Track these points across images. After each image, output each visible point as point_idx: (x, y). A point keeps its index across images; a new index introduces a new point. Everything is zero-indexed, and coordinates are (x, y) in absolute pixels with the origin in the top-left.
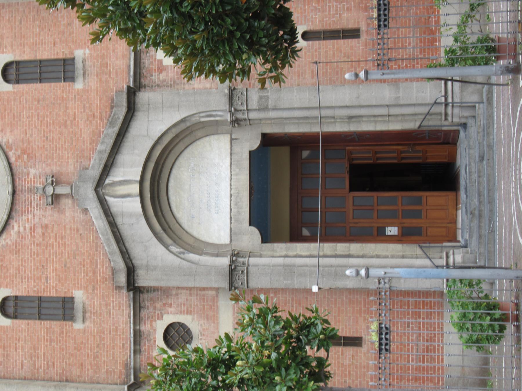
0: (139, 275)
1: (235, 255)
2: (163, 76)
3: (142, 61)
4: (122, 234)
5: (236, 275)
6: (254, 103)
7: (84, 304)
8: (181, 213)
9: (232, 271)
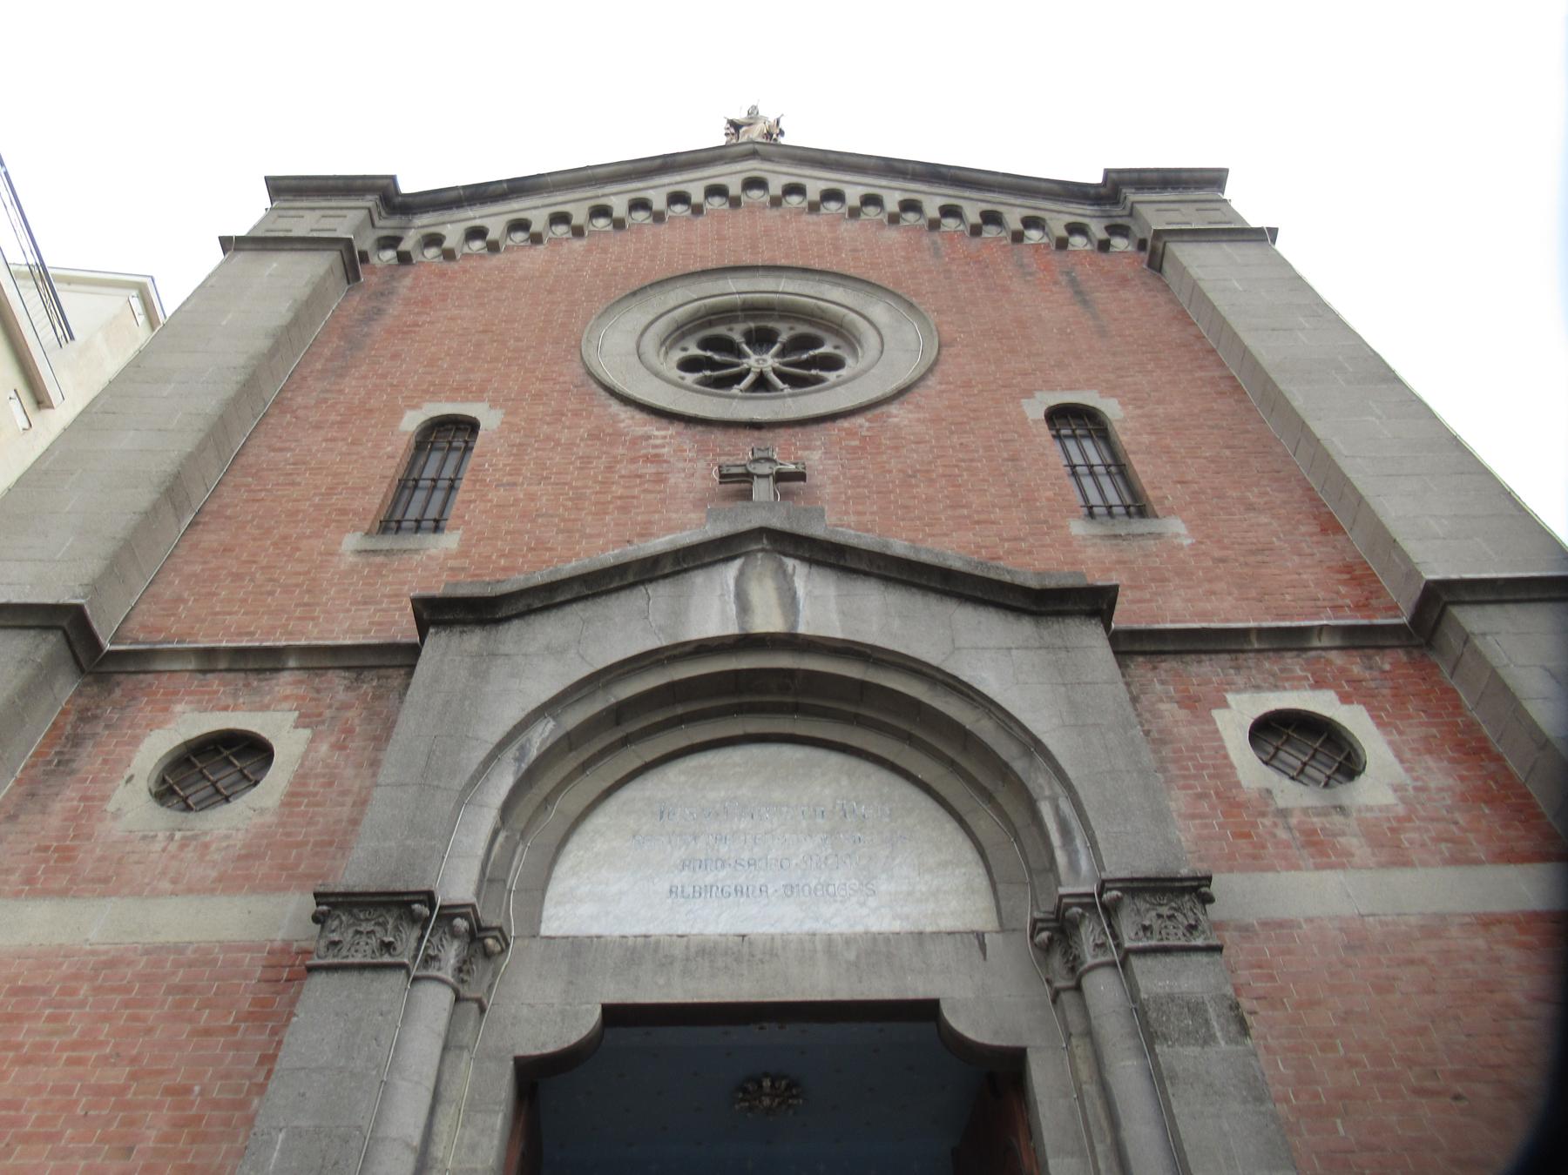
0: (465, 637)
1: (481, 941)
2: (1170, 711)
3: (1203, 657)
4: (614, 596)
5: (383, 925)
6: (1155, 978)
7: (417, 551)
8: (683, 778)
9: (406, 906)
